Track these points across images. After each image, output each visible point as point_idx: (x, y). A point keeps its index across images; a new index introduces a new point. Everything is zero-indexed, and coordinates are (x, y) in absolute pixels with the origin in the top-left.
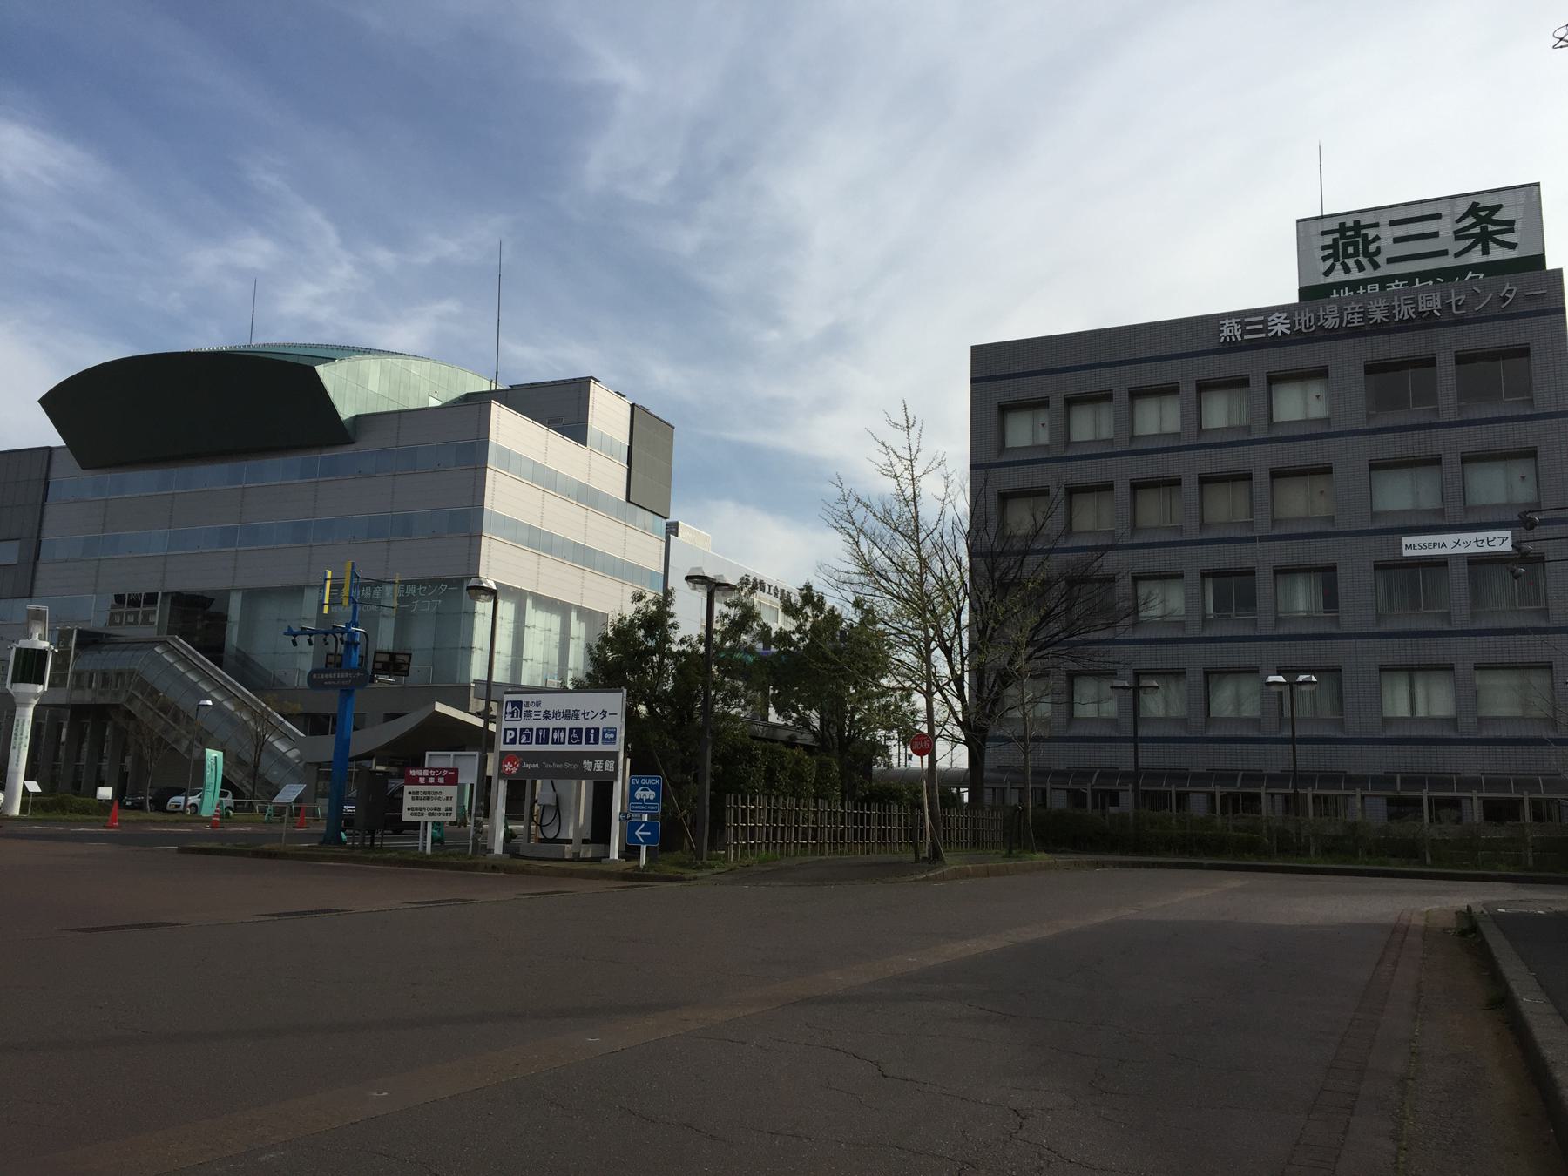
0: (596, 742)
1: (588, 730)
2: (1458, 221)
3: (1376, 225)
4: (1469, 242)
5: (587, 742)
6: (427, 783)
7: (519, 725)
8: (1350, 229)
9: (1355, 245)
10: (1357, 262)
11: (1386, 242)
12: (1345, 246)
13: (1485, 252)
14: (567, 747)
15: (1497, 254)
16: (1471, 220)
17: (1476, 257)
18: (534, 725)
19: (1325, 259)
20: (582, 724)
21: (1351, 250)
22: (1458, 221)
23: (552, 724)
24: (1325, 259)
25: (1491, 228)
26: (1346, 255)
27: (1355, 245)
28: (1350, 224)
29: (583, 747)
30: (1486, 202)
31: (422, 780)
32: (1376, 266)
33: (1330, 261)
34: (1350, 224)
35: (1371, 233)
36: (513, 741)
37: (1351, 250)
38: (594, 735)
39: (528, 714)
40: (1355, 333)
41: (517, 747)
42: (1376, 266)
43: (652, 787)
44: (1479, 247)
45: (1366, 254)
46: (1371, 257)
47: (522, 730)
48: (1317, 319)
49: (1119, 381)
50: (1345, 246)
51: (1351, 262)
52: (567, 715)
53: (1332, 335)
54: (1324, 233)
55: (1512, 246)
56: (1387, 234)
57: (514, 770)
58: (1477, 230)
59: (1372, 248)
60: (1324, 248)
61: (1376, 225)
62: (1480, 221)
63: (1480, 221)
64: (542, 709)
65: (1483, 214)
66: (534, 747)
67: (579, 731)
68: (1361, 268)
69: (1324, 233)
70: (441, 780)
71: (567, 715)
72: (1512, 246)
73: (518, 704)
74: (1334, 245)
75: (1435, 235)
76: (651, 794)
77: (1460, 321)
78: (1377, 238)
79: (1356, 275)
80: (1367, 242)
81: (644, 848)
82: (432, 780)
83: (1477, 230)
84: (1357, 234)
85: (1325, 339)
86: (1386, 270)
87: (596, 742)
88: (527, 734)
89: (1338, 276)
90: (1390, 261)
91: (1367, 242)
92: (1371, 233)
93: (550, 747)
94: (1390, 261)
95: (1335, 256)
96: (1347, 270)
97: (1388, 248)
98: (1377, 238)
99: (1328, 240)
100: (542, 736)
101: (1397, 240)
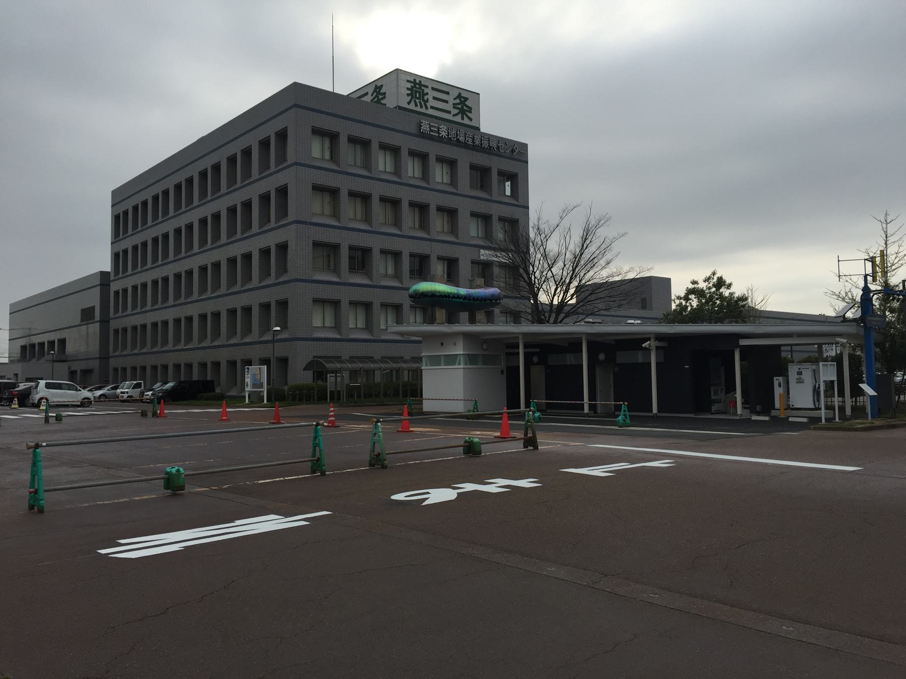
3: (427, 87)
13: (463, 119)
15: (466, 121)
16: (458, 101)
17: (458, 119)
24: (408, 95)
30: (464, 94)
32: (427, 108)
35: (426, 90)
42: (427, 108)
45: (424, 100)
50: (416, 92)
51: (418, 101)
53: (458, 144)
55: (471, 119)
56: (431, 94)
60: (408, 89)
61: (427, 87)
68: (421, 107)
72: (471, 119)
75: (447, 102)
79: (418, 109)
84: (420, 88)
89: (412, 106)
90: (432, 107)
94: (432, 107)
96: (416, 105)
98: (427, 94)
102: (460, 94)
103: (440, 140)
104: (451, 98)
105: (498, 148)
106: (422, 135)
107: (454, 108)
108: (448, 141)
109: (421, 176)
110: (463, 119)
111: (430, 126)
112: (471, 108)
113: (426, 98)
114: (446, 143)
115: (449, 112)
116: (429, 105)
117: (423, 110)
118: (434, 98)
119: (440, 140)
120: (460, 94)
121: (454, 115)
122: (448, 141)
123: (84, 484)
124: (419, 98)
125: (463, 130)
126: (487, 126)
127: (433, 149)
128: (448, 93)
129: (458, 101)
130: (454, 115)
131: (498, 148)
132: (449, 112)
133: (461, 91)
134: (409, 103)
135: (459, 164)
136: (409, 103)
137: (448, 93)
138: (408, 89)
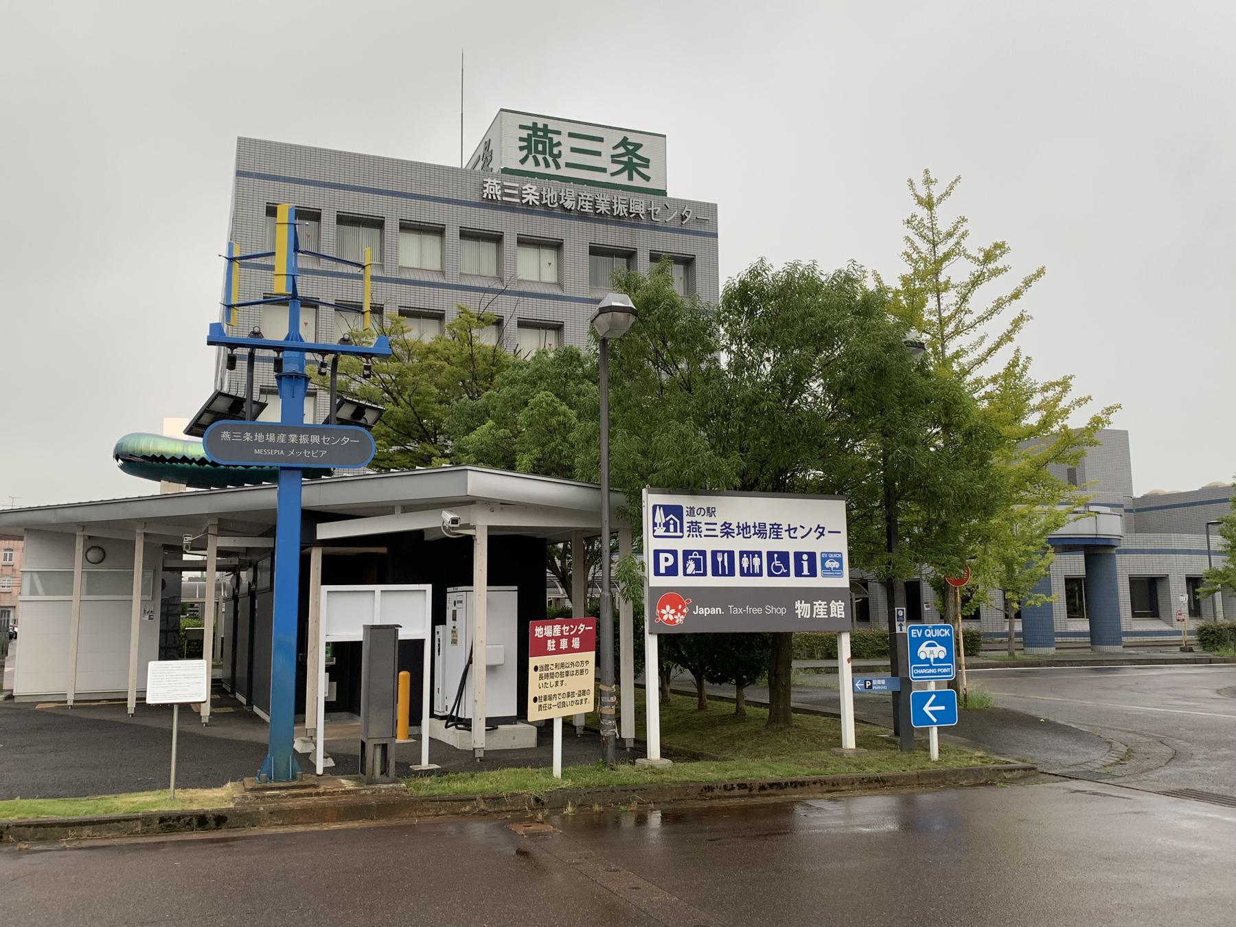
0: (813, 573)
1: (798, 555)
2: (614, 148)
3: (559, 133)
4: (620, 167)
5: (799, 573)
6: (558, 651)
7: (680, 545)
8: (540, 130)
9: (544, 144)
10: (545, 159)
11: (565, 150)
12: (537, 143)
13: (630, 178)
14: (765, 581)
15: (638, 182)
16: (621, 150)
17: (622, 179)
18: (709, 545)
19: (521, 148)
20: (786, 545)
21: (540, 147)
22: (614, 148)
23: (737, 544)
24: (521, 148)
25: (635, 160)
26: (537, 151)
27: (544, 144)
28: (540, 126)
29: (792, 581)
30: (632, 139)
31: (551, 645)
32: (558, 166)
33: (525, 152)
34: (540, 126)
35: (556, 138)
36: (672, 571)
37: (540, 147)
38: (808, 563)
39: (695, 527)
40: (583, 216)
41: (679, 581)
42: (558, 166)
43: (942, 641)
44: (626, 173)
45: (551, 154)
46: (556, 157)
47: (687, 553)
48: (559, 198)
49: (392, 211)
50: (537, 143)
51: (540, 157)
52: (761, 531)
53: (566, 213)
54: (521, 127)
55: (647, 178)
56: (567, 143)
57: (680, 619)
58: (625, 159)
59: (556, 151)
60: (521, 139)
61: (559, 133)
62: (628, 152)
63: (628, 152)
64: (719, 519)
65: (631, 148)
66: (710, 581)
67: (784, 556)
68: (547, 165)
69: (521, 127)
70: (576, 643)
71: (761, 531)
72: (647, 178)
73: (677, 511)
74: (528, 140)
75: (598, 154)
76: (940, 652)
77: (654, 227)
78: (559, 144)
79: (542, 169)
80: (552, 145)
81: (934, 731)
82: (564, 644)
83: (625, 159)
84: (545, 136)
85: (561, 216)
86: (565, 172)
87: (813, 573)
88: (697, 560)
89: (530, 166)
90: (568, 165)
91: (552, 145)
92: (556, 138)
93: (737, 581)
94: (568, 165)
95: (528, 148)
96: (537, 164)
97: (567, 156)
98: (559, 144)
99: (524, 134)
100: (724, 564)
101: (573, 150)
102: (625, 139)
103: (528, 209)
104: (607, 149)
105: (649, 213)
106: (490, 203)
107: (613, 162)
108: (545, 210)
109: (494, 273)
110: (630, 178)
111: (503, 187)
112: (648, 161)
113: (556, 151)
114: (539, 213)
115: (604, 170)
116: (561, 161)
117: (552, 170)
118: (573, 150)
119: (528, 209)
120: (625, 139)
121: (612, 174)
122: (545, 210)
123: (1073, 639)
124: (543, 152)
125: (572, 189)
126: (678, 189)
127: (511, 225)
128: (601, 140)
129: (621, 150)
130: (612, 174)
131: (649, 213)
132: (604, 170)
133: (627, 134)
134: (523, 161)
135: (506, 238)
136: (523, 161)
137: (601, 140)
138: (521, 139)
